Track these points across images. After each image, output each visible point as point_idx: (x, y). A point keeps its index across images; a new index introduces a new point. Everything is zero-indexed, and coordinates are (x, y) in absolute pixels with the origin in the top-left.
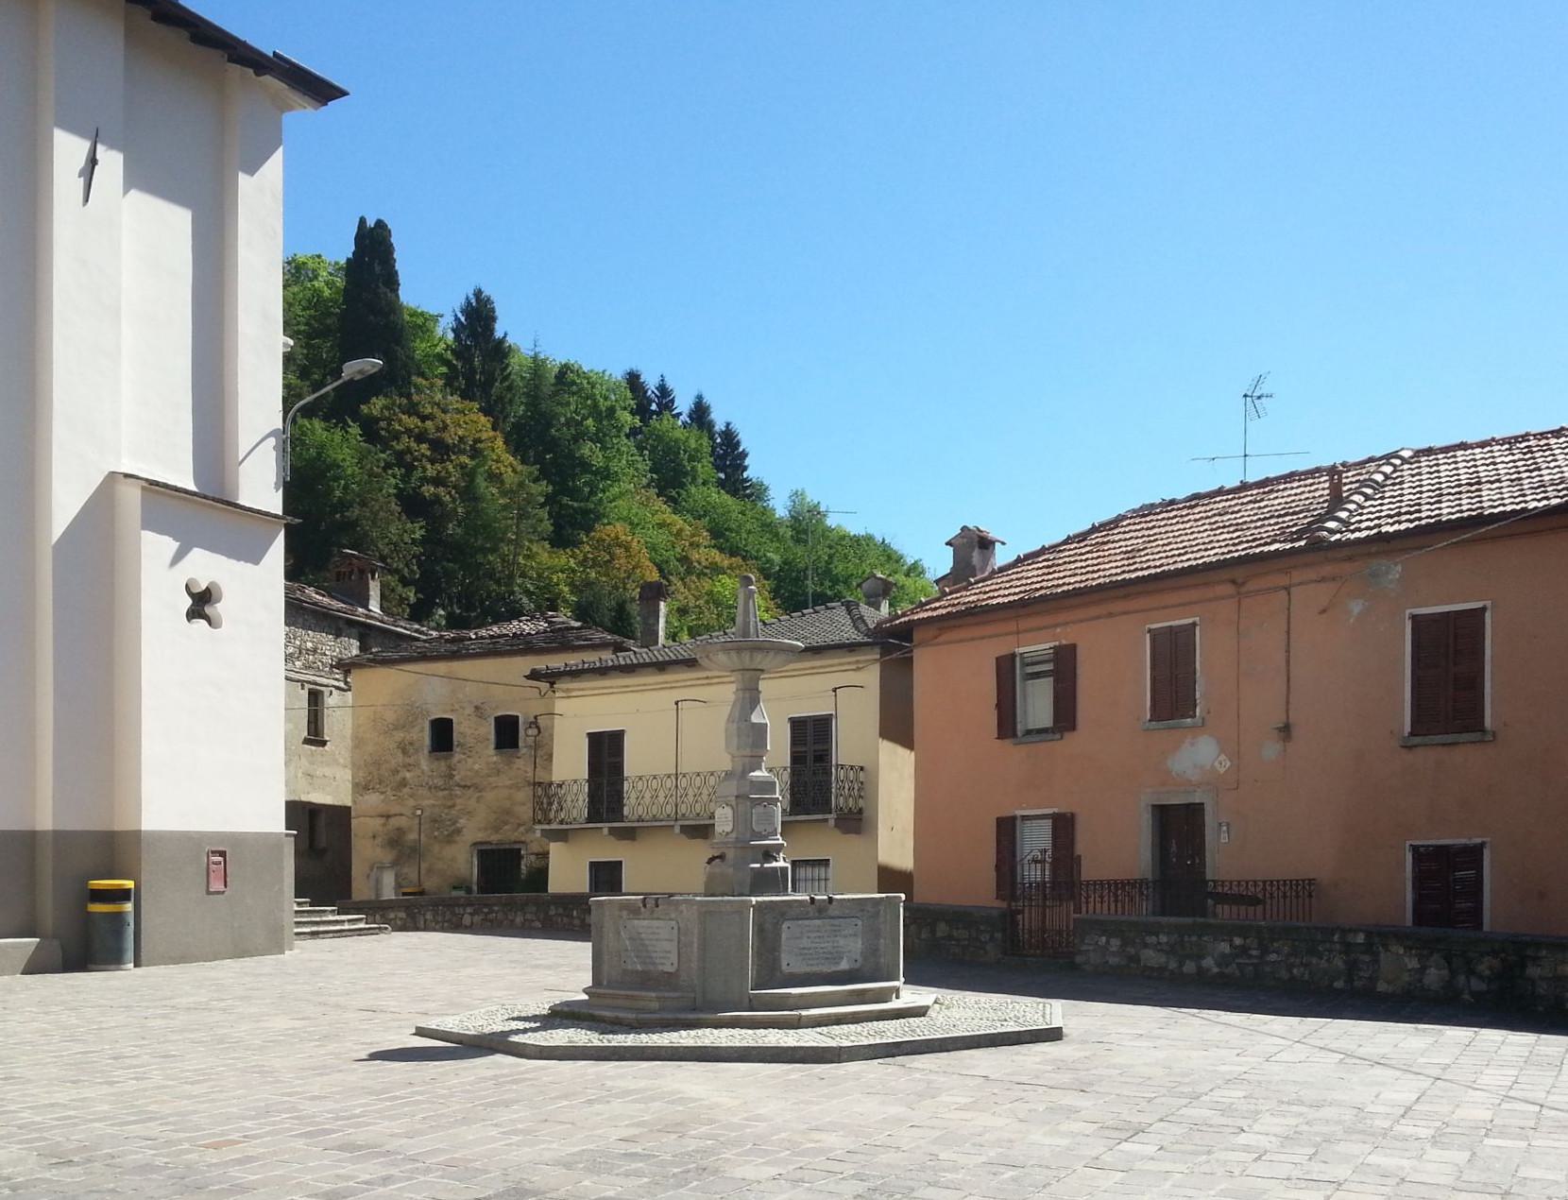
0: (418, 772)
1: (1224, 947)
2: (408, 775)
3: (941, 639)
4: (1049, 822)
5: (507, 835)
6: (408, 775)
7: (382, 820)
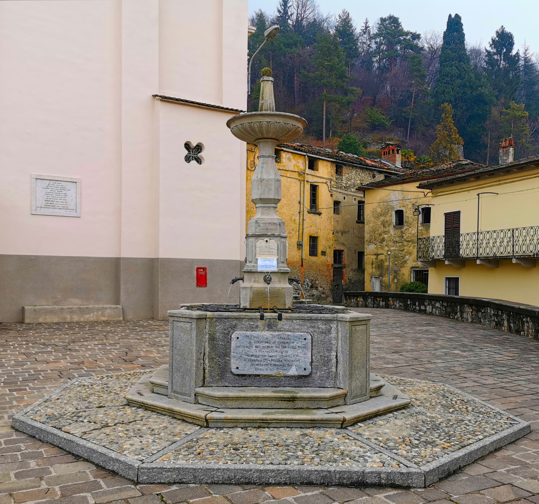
0: (389, 235)
2: (385, 236)
6: (385, 236)
7: (374, 257)
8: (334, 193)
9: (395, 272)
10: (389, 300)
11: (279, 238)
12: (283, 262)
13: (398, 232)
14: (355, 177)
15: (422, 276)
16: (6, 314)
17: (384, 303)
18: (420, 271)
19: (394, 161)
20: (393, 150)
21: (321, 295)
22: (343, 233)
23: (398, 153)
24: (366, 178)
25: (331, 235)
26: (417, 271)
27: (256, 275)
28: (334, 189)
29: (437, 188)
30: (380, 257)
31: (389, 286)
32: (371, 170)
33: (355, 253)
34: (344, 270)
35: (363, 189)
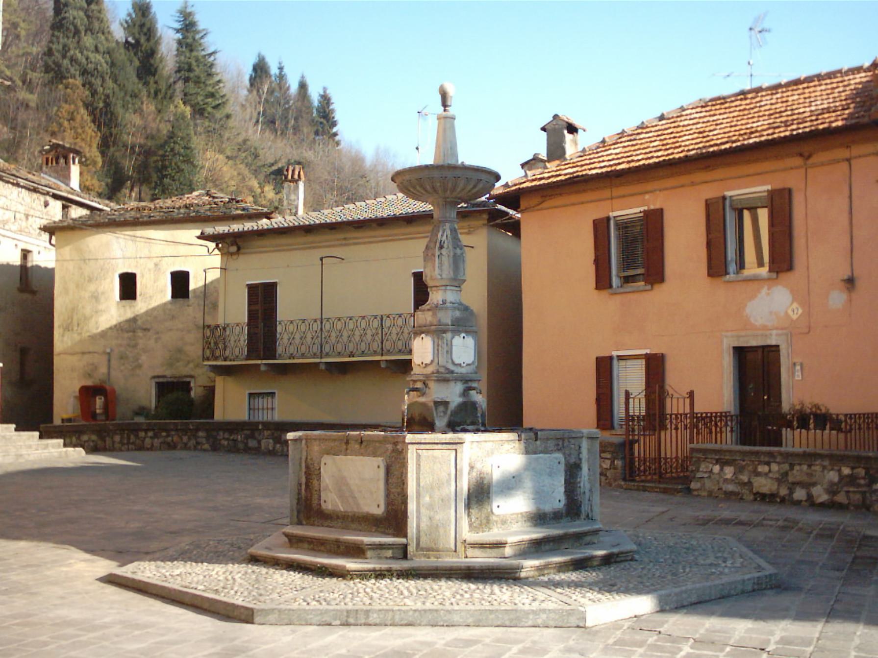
1: (833, 476)
3: (544, 205)
4: (643, 362)
5: (183, 370)
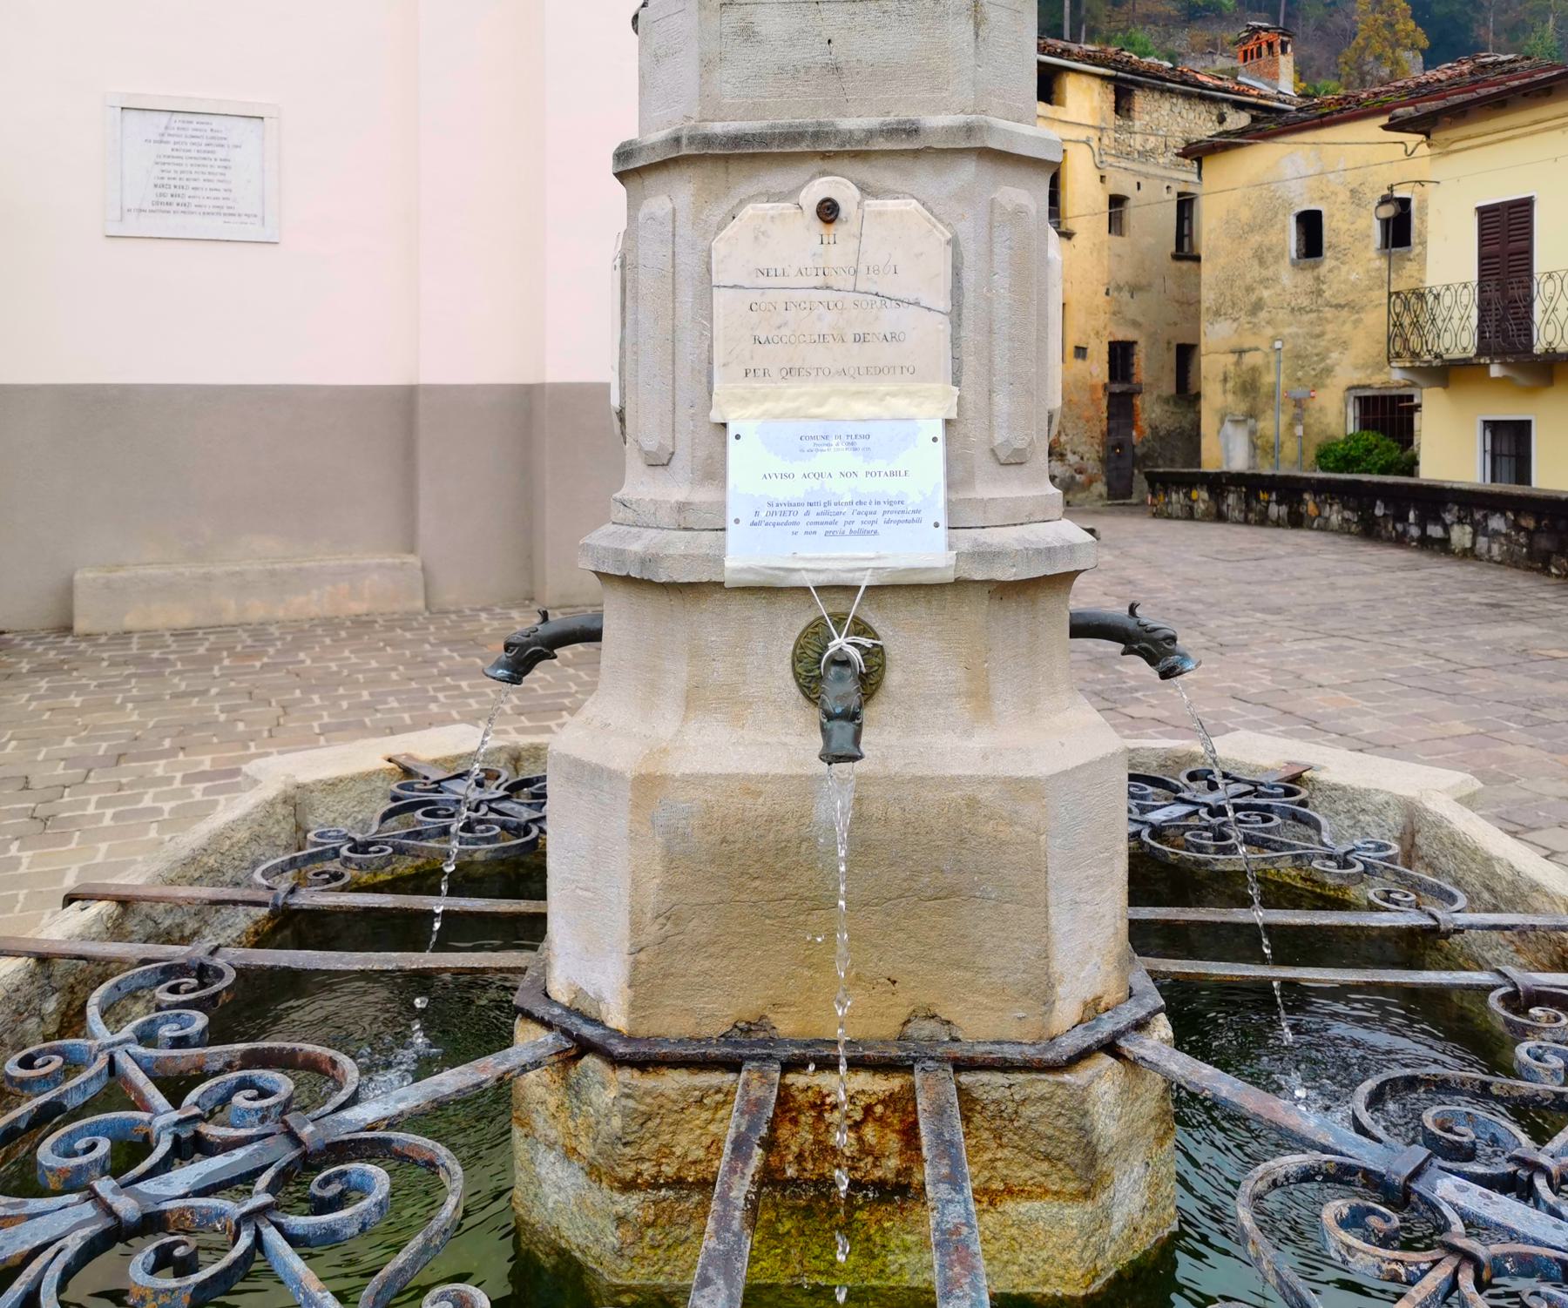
0: (1278, 289)
2: (1266, 294)
7: (1233, 358)
8: (1108, 172)
9: (1298, 403)
10: (1301, 501)
11: (968, 171)
12: (1015, 461)
13: (1306, 279)
14: (1167, 121)
15: (1388, 417)
16: (12, 602)
17: (1284, 510)
18: (1375, 398)
19: (1274, 76)
20: (1270, 46)
21: (1073, 478)
22: (1134, 290)
23: (1284, 51)
24: (1200, 123)
25: (1101, 298)
26: (1367, 398)
27: (711, 625)
28: (1111, 160)
29: (1451, 126)
30: (1249, 359)
31: (1273, 449)
32: (1213, 100)
33: (1169, 349)
34: (1138, 401)
35: (1197, 153)
